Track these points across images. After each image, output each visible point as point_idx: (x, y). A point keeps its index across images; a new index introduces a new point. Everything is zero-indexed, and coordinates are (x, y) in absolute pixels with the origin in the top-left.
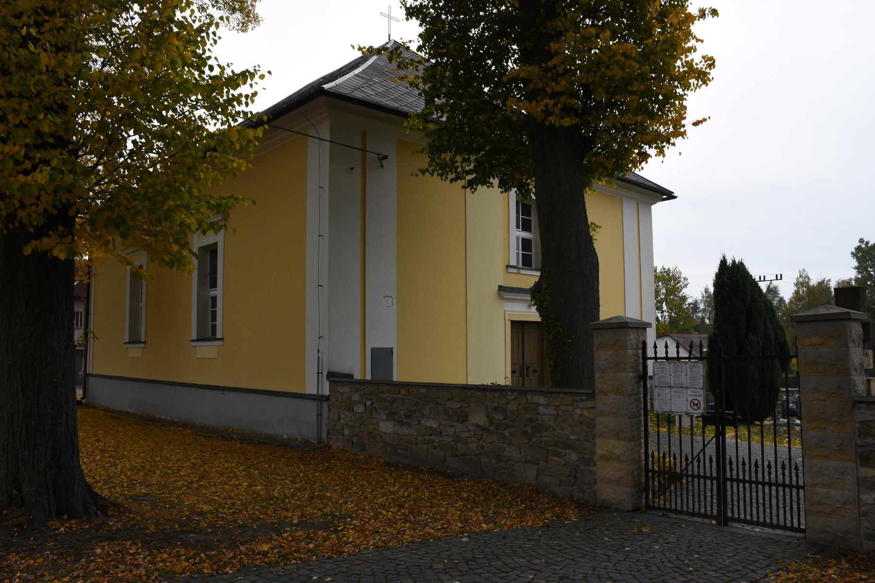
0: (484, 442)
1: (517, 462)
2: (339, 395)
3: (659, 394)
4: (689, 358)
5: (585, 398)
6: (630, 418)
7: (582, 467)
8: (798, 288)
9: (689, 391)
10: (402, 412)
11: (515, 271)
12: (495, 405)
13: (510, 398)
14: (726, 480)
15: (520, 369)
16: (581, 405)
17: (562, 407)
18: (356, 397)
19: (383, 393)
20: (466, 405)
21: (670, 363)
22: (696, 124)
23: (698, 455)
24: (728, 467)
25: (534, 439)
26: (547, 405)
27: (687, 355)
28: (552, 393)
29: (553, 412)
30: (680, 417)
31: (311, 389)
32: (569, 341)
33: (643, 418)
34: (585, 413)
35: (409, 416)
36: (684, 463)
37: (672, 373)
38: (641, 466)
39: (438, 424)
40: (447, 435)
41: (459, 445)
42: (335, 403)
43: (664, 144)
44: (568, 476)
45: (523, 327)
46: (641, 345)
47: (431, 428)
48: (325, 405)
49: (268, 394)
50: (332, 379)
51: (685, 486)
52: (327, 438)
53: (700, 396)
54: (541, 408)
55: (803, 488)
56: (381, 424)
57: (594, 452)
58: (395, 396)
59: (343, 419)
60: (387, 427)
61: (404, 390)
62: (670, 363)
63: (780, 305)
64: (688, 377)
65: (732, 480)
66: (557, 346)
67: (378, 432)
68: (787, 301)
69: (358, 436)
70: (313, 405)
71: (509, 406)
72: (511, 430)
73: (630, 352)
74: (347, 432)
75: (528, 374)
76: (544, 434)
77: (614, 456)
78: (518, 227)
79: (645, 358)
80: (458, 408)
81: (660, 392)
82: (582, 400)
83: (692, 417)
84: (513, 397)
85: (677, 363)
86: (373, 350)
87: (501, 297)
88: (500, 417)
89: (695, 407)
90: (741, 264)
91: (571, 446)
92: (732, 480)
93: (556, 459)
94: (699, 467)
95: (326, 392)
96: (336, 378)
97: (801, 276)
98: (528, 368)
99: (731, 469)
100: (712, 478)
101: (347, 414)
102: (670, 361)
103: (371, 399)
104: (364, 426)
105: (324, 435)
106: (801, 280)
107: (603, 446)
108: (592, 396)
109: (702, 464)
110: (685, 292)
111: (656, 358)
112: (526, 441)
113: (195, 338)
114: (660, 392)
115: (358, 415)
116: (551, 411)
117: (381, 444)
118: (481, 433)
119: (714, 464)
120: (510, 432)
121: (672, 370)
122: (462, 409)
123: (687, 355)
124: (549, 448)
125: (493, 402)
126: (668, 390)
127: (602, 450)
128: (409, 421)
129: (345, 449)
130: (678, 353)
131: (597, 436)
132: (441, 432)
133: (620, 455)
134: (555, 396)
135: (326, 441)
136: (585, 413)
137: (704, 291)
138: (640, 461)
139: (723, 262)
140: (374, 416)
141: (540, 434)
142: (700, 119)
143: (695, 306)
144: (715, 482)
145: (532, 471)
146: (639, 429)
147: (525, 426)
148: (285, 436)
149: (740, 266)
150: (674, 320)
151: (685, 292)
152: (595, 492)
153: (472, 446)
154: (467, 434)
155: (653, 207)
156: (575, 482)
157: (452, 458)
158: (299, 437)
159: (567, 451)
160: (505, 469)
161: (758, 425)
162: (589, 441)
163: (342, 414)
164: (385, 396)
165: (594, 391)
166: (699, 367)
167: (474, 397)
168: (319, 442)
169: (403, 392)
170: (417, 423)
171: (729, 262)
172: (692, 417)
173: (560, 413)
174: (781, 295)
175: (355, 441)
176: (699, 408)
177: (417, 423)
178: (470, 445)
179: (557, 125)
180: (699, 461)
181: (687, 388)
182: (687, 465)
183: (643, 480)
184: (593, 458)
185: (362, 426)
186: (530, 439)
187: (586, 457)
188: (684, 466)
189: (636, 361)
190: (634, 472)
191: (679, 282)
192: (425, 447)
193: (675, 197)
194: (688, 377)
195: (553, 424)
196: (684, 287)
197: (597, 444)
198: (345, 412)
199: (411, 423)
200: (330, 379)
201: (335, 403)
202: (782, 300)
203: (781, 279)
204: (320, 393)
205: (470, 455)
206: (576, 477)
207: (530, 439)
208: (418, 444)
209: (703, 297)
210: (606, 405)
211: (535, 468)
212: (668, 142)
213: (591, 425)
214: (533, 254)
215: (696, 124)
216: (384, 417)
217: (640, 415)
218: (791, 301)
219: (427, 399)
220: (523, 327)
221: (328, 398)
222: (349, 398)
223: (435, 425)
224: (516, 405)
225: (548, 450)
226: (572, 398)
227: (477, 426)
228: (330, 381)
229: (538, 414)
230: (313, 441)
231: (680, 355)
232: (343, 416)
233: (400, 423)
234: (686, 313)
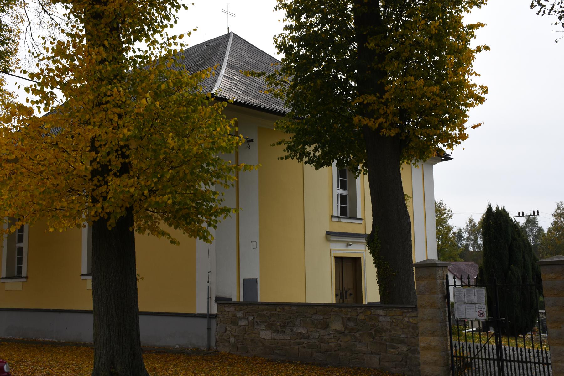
0: (341, 341)
1: (365, 354)
2: (225, 313)
3: (458, 308)
4: (462, 285)
5: (410, 310)
6: (440, 322)
7: (410, 355)
8: (556, 219)
9: (477, 306)
10: (278, 324)
11: (337, 219)
12: (349, 316)
13: (359, 311)
14: (503, 360)
15: (341, 293)
16: (408, 315)
17: (396, 317)
18: (240, 314)
19: (263, 311)
20: (327, 317)
21: (464, 289)
22: (474, 127)
23: (484, 346)
24: (504, 352)
25: (376, 338)
26: (386, 316)
27: (460, 284)
28: (388, 307)
29: (390, 320)
30: (472, 322)
31: (202, 309)
32: (393, 274)
33: (448, 323)
34: (411, 320)
35: (284, 326)
36: (476, 350)
37: (465, 295)
38: (448, 354)
39: (306, 330)
40: (313, 338)
41: (322, 345)
42: (222, 319)
43: (454, 143)
44: (401, 361)
45: (342, 261)
46: (445, 277)
47: (301, 334)
48: (214, 322)
49: (145, 315)
50: (219, 302)
51: (474, 371)
52: (216, 346)
53: (484, 308)
54: (381, 317)
55: (550, 364)
56: (261, 333)
57: (418, 345)
58: (272, 313)
59: (229, 331)
60: (266, 334)
61: (280, 308)
62: (464, 289)
63: (539, 234)
64: (476, 297)
65: (507, 361)
66: (385, 277)
67: (259, 339)
68: (546, 231)
69: (242, 342)
70: (205, 321)
71: (358, 317)
72: (360, 333)
73: (439, 281)
74: (232, 340)
75: (346, 296)
76: (384, 334)
77: (431, 347)
78: (338, 187)
79: (448, 285)
80: (322, 319)
81: (459, 306)
82: (408, 312)
83: (479, 322)
84: (361, 311)
85: (468, 288)
86: (244, 280)
87: (328, 240)
88: (352, 324)
89: (481, 316)
90: (504, 210)
91: (402, 342)
92: (507, 361)
93: (392, 350)
94: (485, 353)
95: (214, 311)
96: (222, 301)
97: (559, 208)
98: (346, 292)
99: (506, 354)
100: (494, 360)
101: (233, 327)
102: (464, 287)
103: (253, 315)
104: (247, 335)
105: (213, 344)
106: (559, 211)
107: (424, 341)
108: (415, 309)
109: (487, 351)
110: (450, 222)
111: (455, 285)
112: (372, 340)
113: (86, 273)
114: (459, 306)
115: (242, 327)
116: (388, 319)
117: (261, 347)
118: (338, 335)
119: (495, 351)
120: (360, 334)
121: (465, 293)
122: (324, 320)
123: (460, 284)
124: (387, 343)
125: (347, 314)
126: (463, 305)
127: (423, 343)
128: (284, 329)
129: (231, 352)
130: (455, 282)
131: (419, 335)
132: (309, 336)
133: (435, 346)
134: (390, 309)
135: (215, 348)
136: (411, 320)
137: (468, 220)
138: (447, 350)
139: (489, 209)
140: (255, 328)
141: (381, 334)
142: (477, 123)
143: (459, 235)
144: (496, 362)
145: (376, 359)
146: (446, 329)
147: (370, 330)
148: (177, 346)
149: (503, 212)
150: (441, 248)
151: (450, 222)
152: (419, 371)
153: (333, 345)
154: (329, 337)
155: (434, 166)
156: (406, 365)
157: (317, 354)
158: (190, 346)
159: (400, 345)
160: (357, 359)
161: (522, 337)
162: (414, 338)
163: (229, 327)
164: (265, 313)
165: (416, 306)
166: (483, 291)
167: (334, 312)
168: (209, 348)
169: (278, 310)
170: (290, 331)
171: (494, 209)
172: (479, 322)
173: (394, 320)
174: (539, 225)
175: (239, 346)
176: (483, 316)
177: (290, 331)
178: (331, 344)
179: (387, 135)
180: (485, 349)
181: (475, 303)
182: (478, 352)
183: (450, 362)
184: (417, 349)
185: (246, 335)
186: (374, 338)
187: (412, 348)
188: (476, 353)
189: (442, 287)
190: (444, 357)
191: (445, 213)
192: (297, 347)
193: (451, 159)
194: (476, 297)
195: (390, 328)
196: (449, 218)
197: (419, 340)
198: (230, 325)
199: (286, 331)
200: (218, 302)
201: (222, 319)
202: (540, 229)
203: (538, 214)
204: (209, 313)
205: (331, 351)
206: (406, 362)
207: (374, 338)
208: (291, 346)
209: (467, 226)
210: (425, 315)
211: (378, 357)
212: (457, 142)
213: (415, 327)
214: (348, 206)
215: (474, 127)
216: (264, 328)
217: (446, 321)
218: (549, 231)
219: (298, 314)
220: (342, 261)
221: (216, 316)
222: (235, 316)
223: (304, 332)
224: (363, 316)
225: (386, 345)
226: (402, 311)
227: (336, 331)
228: (217, 303)
229: (379, 321)
230: (203, 349)
231: (456, 284)
232: (229, 329)
233: (277, 331)
234: (452, 242)
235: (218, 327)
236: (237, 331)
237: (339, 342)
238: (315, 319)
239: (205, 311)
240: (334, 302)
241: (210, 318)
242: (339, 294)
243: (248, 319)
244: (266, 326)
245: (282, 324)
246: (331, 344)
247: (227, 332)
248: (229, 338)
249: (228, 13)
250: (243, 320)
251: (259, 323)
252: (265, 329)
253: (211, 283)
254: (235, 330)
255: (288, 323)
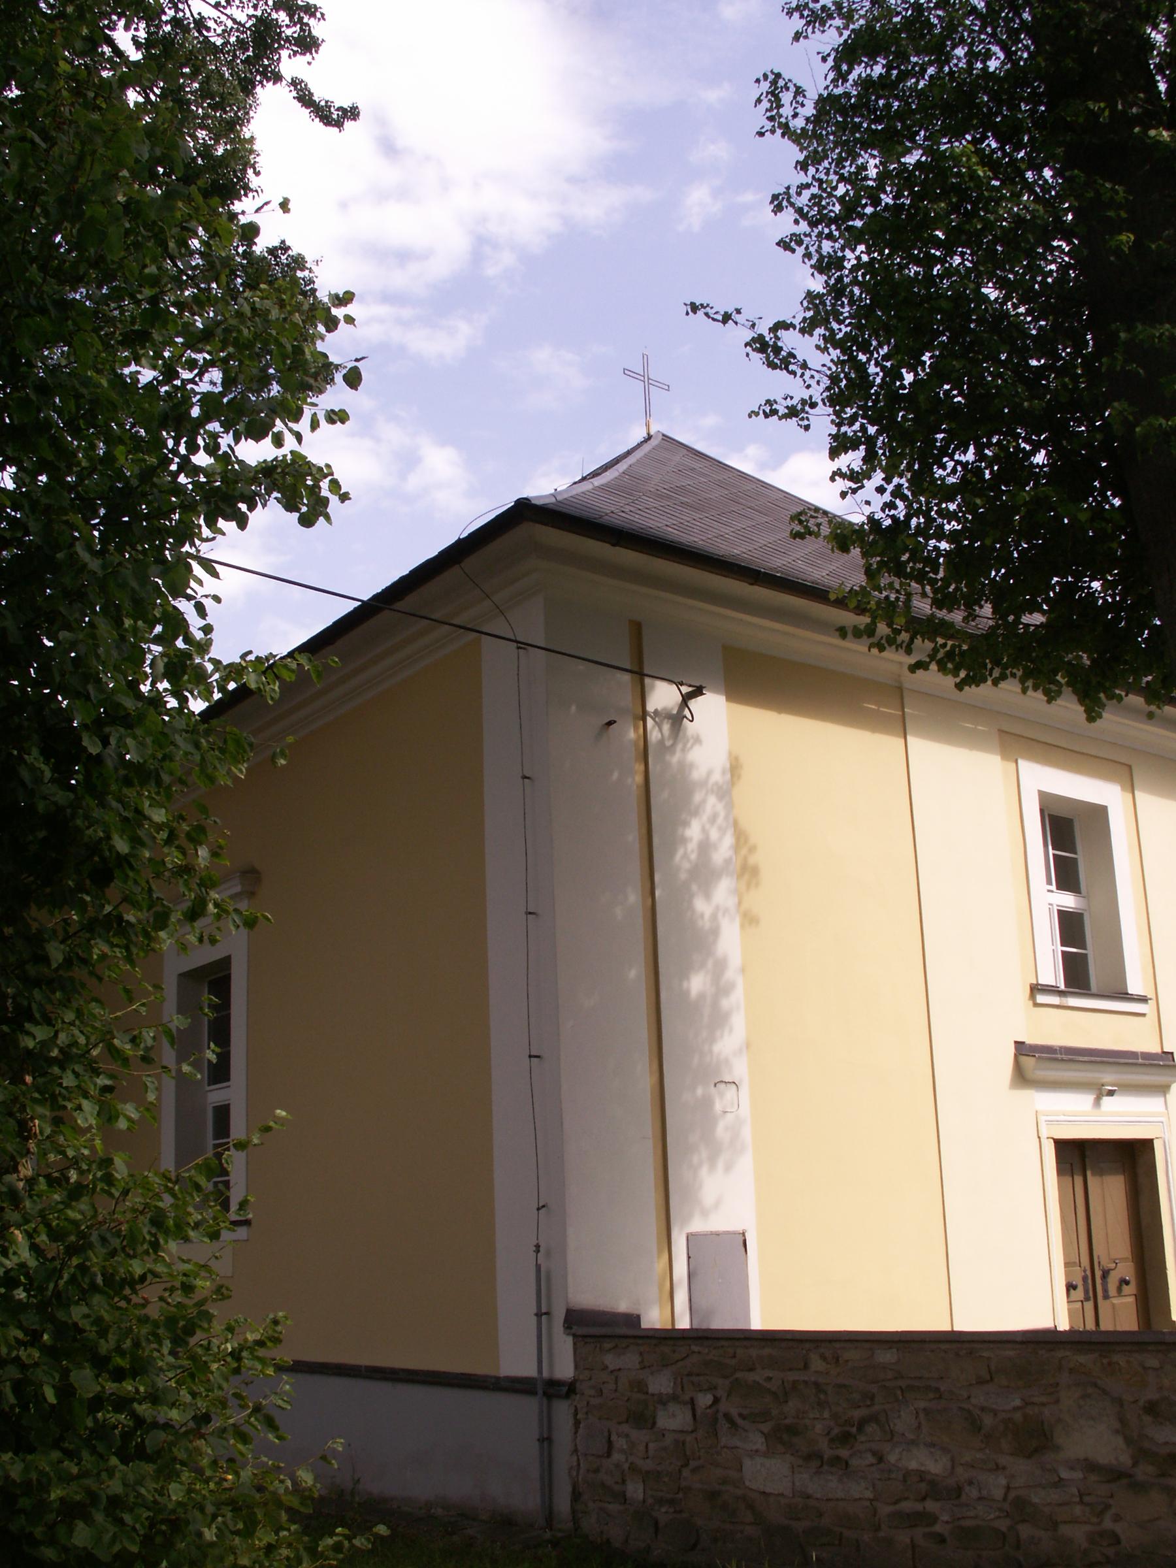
0: (1117, 1518)
11: (1055, 1000)
12: (1151, 1394)
15: (1085, 1279)
18: (661, 1383)
19: (751, 1370)
20: (1043, 1399)
40: (980, 1499)
41: (1025, 1531)
47: (921, 1475)
48: (563, 1411)
49: (321, 1373)
58: (792, 1376)
69: (671, 1502)
70: (530, 1406)
75: (1105, 1291)
78: (1049, 882)
80: (1016, 1409)
95: (565, 1369)
98: (1105, 1274)
101: (635, 1434)
103: (712, 1388)
104: (694, 1471)
105: (563, 1504)
128: (844, 1453)
132: (959, 1490)
153: (1078, 1534)
167: (1071, 1371)
169: (817, 1364)
185: (686, 1473)
198: (625, 1428)
199: (854, 1462)
200: (575, 1329)
204: (545, 1374)
216: (758, 1442)
221: (569, 1389)
223: (935, 1466)
227: (1090, 1466)
228: (574, 1336)
232: (620, 1443)
235: (581, 1431)
236: (651, 1453)
237: (1108, 1524)
238: (983, 1409)
239: (527, 1369)
240: (1064, 1325)
241: (548, 1396)
242: (1078, 1281)
243: (692, 1402)
244: (766, 1436)
245: (836, 1431)
246: (1065, 1530)
247: (616, 1457)
248: (624, 1482)
249: (647, 381)
250: (673, 1407)
251: (739, 1421)
252: (763, 1448)
253: (548, 1254)
254: (642, 1448)
255: (861, 1424)
